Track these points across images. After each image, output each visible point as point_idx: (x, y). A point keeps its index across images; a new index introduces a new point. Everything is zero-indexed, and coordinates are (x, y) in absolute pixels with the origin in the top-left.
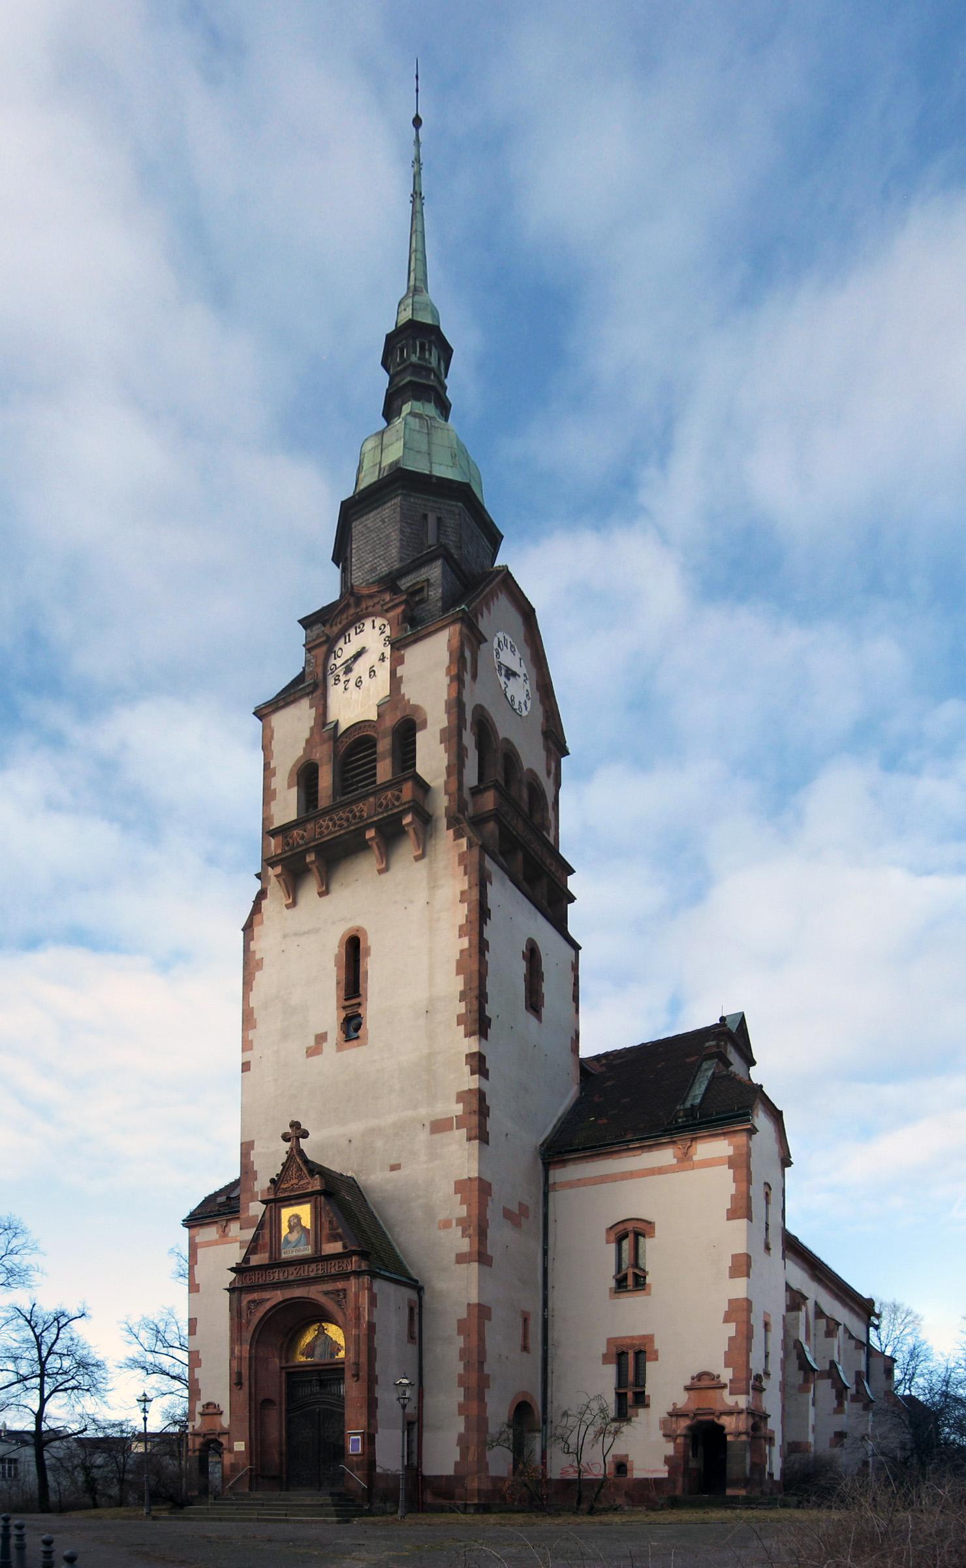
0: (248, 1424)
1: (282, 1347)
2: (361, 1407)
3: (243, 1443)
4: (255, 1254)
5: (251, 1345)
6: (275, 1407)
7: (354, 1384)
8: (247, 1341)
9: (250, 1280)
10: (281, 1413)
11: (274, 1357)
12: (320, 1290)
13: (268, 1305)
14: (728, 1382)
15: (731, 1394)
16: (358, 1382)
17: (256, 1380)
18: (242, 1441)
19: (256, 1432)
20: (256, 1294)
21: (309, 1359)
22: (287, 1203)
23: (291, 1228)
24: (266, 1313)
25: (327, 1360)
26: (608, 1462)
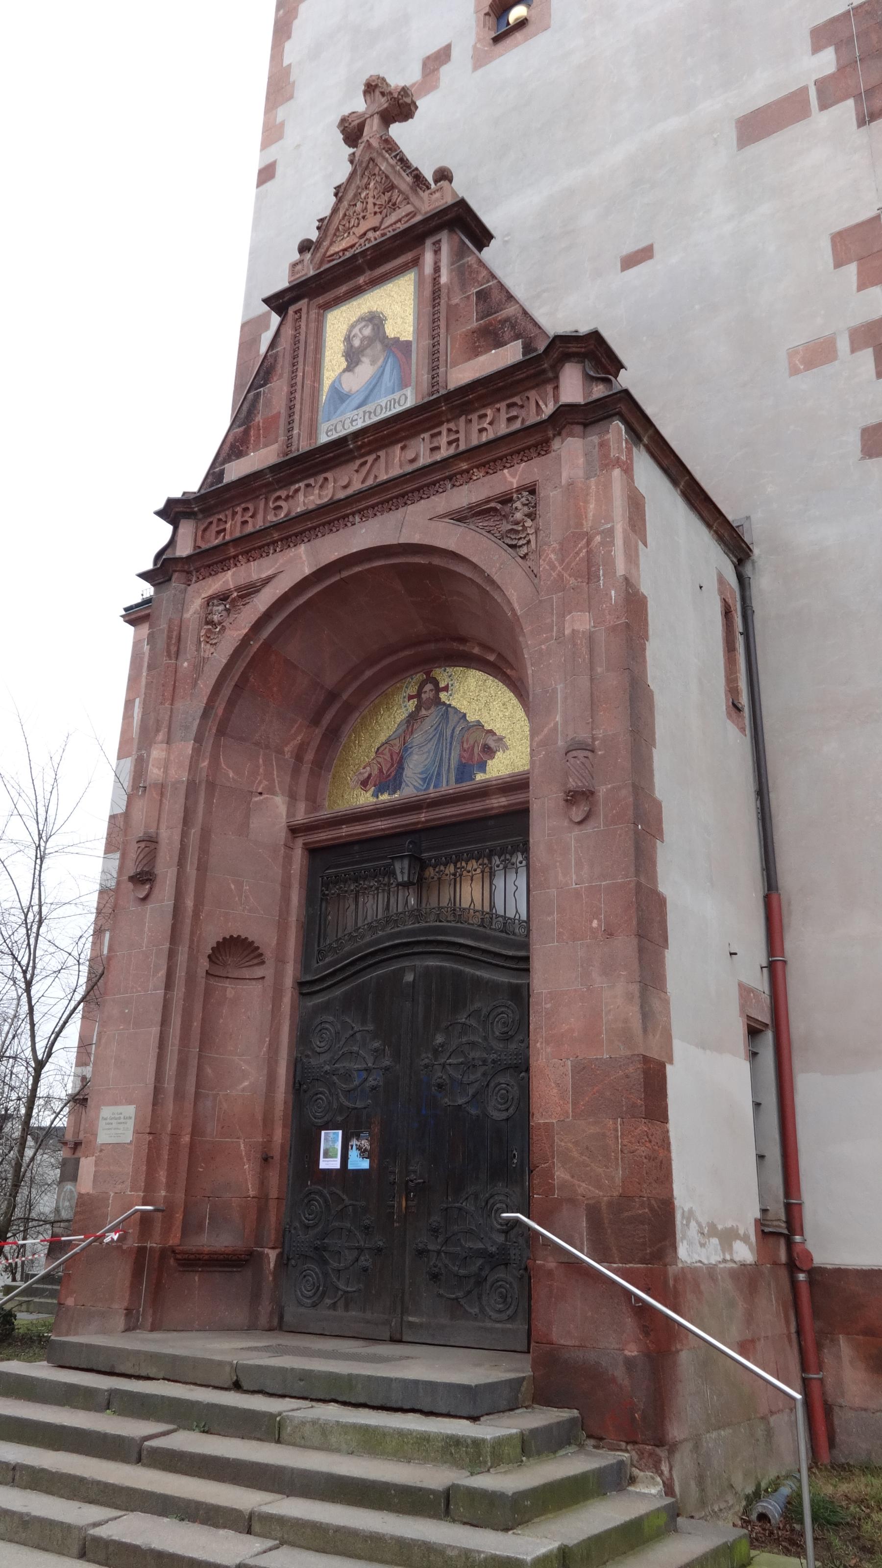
0: (155, 1030)
1: (299, 757)
2: (610, 933)
5: (199, 739)
6: (259, 972)
7: (573, 836)
8: (187, 728)
9: (218, 533)
10: (278, 992)
11: (274, 793)
12: (441, 510)
13: (263, 601)
16: (589, 828)
17: (202, 868)
19: (183, 1064)
20: (230, 573)
21: (385, 797)
24: (258, 626)
25: (448, 786)
26: (336, 1157)
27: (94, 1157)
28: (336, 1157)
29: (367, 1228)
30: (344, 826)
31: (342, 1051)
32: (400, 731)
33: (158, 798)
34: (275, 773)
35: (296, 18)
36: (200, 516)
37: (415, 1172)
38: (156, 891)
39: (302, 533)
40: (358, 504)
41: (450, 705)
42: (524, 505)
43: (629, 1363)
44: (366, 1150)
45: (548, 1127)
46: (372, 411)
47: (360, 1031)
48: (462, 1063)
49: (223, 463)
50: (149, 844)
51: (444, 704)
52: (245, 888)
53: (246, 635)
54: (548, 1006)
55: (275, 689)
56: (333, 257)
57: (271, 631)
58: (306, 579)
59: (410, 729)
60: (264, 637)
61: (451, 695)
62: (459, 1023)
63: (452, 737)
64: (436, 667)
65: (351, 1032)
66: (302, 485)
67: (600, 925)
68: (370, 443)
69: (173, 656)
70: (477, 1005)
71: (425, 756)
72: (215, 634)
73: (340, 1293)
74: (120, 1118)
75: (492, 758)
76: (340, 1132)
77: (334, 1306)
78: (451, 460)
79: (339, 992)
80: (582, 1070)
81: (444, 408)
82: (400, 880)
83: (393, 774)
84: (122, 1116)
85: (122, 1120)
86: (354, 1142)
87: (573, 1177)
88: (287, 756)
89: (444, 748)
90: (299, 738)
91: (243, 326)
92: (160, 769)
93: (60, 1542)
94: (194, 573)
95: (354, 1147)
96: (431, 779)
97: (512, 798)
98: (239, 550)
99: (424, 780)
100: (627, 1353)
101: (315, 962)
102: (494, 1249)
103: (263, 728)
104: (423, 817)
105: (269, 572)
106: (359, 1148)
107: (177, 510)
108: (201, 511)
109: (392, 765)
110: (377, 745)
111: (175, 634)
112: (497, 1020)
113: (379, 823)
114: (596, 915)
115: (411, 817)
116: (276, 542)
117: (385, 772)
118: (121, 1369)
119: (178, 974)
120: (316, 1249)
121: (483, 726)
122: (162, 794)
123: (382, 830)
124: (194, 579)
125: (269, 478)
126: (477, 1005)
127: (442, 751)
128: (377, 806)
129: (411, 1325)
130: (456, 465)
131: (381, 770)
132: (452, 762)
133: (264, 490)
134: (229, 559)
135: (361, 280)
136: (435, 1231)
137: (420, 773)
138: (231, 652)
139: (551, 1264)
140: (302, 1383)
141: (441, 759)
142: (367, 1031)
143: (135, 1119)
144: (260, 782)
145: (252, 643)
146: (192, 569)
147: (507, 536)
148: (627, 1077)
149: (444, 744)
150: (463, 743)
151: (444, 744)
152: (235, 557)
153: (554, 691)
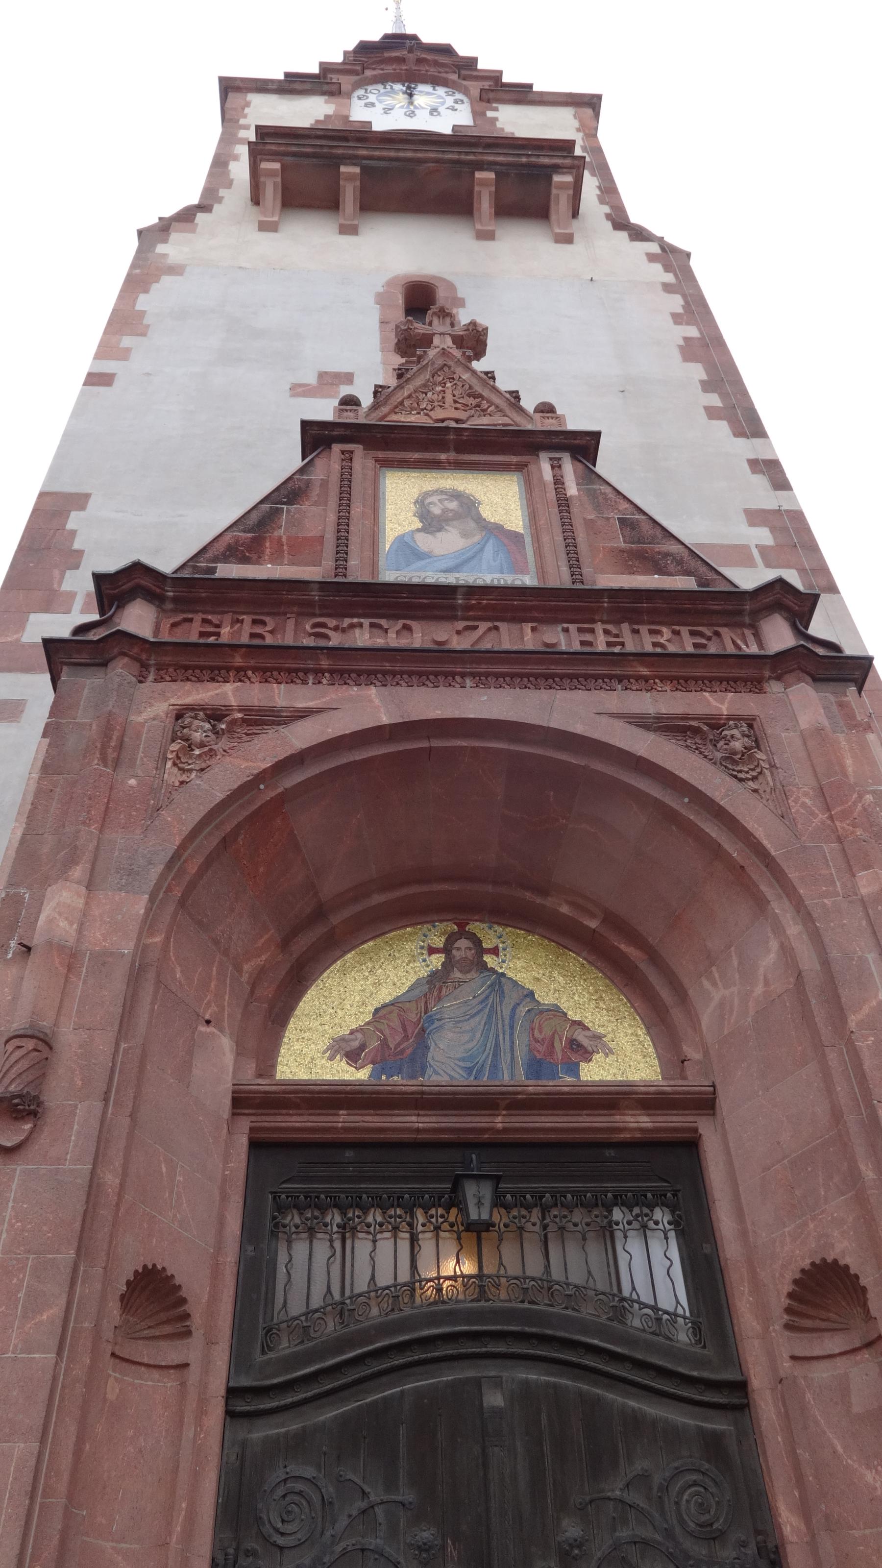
6: (172, 1353)
30: (341, 1112)
31: (343, 1545)
32: (417, 992)
33: (63, 971)
34: (227, 998)
35: (157, 281)
36: (169, 606)
38: (44, 1139)
39: (375, 673)
40: (474, 666)
41: (503, 975)
42: (744, 735)
47: (382, 1503)
49: (216, 559)
50: (41, 1045)
52: (178, 1178)
53: (265, 771)
55: (261, 870)
57: (299, 780)
58: (380, 729)
59: (435, 994)
61: (504, 962)
62: (609, 1499)
63: (512, 1017)
64: (477, 921)
65: (363, 1505)
66: (366, 622)
68: (486, 608)
69: (110, 763)
70: (640, 1465)
71: (467, 1037)
72: (191, 758)
78: (631, 658)
79: (328, 1414)
81: (606, 605)
82: (474, 1216)
83: (409, 1051)
88: (245, 978)
89: (500, 1031)
90: (264, 958)
91: (42, 495)
92: (71, 924)
94: (152, 670)
97: (660, 1119)
98: (252, 663)
99: (469, 1070)
101: (258, 1351)
103: (229, 920)
104: (499, 1121)
105: (311, 704)
107: (143, 582)
108: (175, 600)
109: (406, 1038)
110: (377, 1004)
111: (116, 735)
112: (685, 1497)
113: (414, 1119)
115: (477, 1119)
117: (392, 1046)
119: (72, 1325)
121: (565, 1014)
122: (70, 968)
123: (418, 1130)
124: (151, 677)
125: (316, 596)
126: (640, 1465)
127: (498, 1036)
128: (424, 1088)
130: (632, 666)
131: (384, 1043)
132: (518, 1053)
133: (295, 609)
134: (228, 669)
135: (443, 456)
137: (463, 1059)
138: (235, 787)
141: (497, 1045)
144: (208, 1005)
145: (262, 787)
146: (152, 662)
147: (721, 764)
149: (500, 1026)
150: (533, 1029)
151: (500, 1026)
152: (239, 670)
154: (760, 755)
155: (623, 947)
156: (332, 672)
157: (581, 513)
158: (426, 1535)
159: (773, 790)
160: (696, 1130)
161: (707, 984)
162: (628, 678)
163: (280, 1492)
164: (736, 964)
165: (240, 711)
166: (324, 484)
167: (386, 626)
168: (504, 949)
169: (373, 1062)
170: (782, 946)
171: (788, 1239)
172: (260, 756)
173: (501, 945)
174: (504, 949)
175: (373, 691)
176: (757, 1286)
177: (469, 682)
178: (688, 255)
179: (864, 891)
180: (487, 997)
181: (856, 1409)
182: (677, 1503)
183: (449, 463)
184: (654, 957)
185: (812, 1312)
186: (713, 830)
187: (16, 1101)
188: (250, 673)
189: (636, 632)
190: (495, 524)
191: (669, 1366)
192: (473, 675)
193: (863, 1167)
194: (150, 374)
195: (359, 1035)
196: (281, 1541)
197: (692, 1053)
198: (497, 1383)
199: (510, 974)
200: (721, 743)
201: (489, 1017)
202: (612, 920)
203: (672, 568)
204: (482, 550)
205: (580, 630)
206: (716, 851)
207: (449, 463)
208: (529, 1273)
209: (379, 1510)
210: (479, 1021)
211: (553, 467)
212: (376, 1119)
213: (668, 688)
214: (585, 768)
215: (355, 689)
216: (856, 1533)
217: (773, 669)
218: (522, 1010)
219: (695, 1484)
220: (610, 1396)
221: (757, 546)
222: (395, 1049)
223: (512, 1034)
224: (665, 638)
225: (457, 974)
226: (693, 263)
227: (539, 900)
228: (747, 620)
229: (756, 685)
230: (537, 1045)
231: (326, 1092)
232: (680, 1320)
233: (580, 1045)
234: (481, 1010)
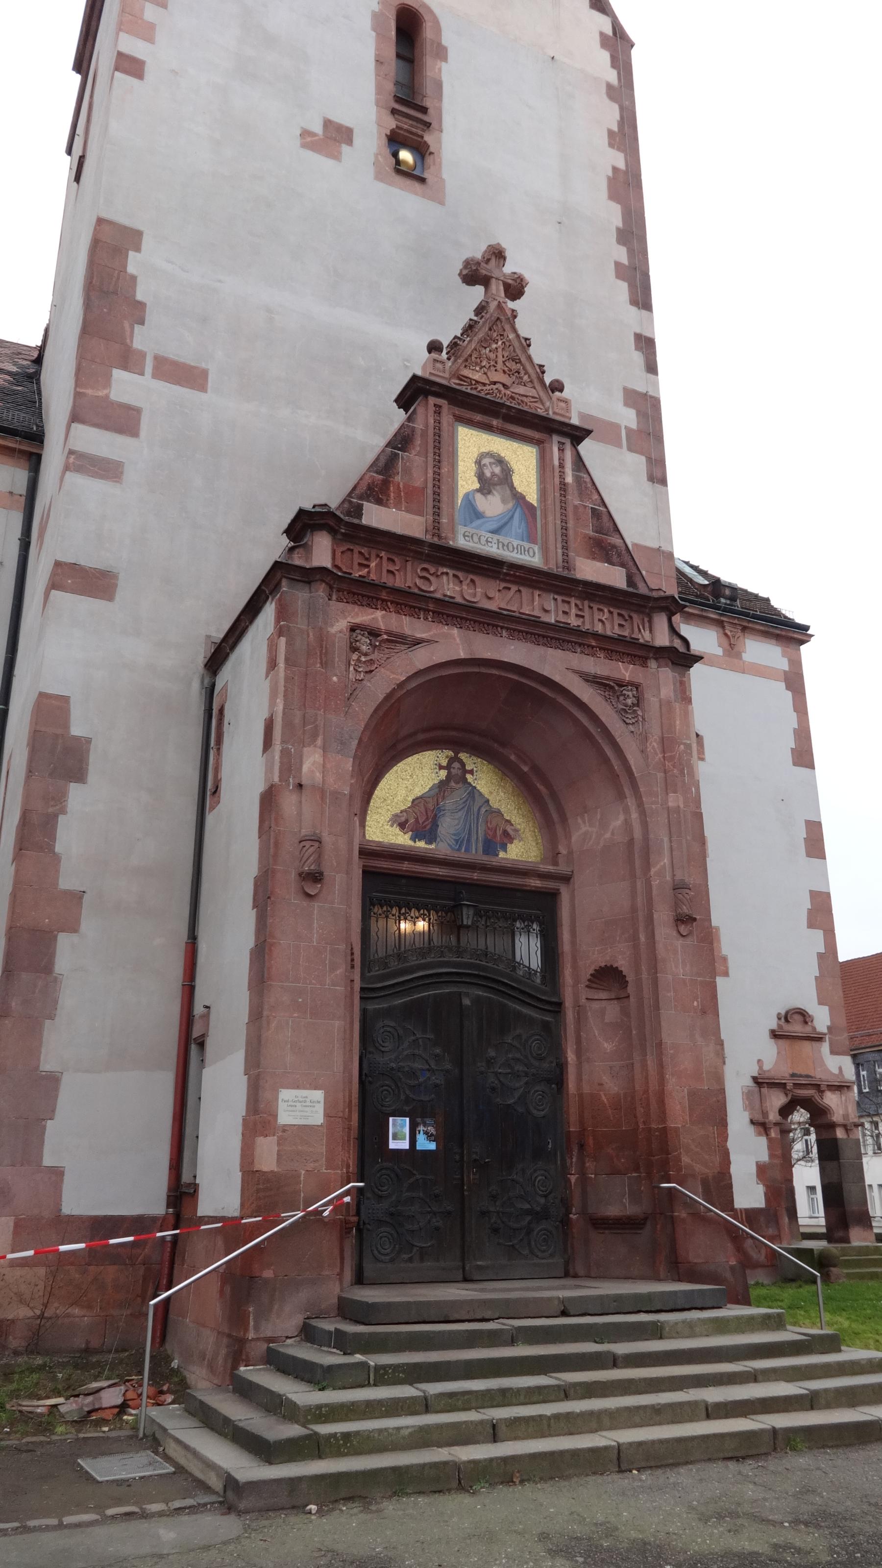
3: (318, 1095)
4: (379, 502)
7: (679, 943)
13: (422, 658)
14: (825, 1031)
15: (833, 1052)
18: (316, 1088)
21: (421, 844)
22: (478, 417)
23: (486, 486)
25: (476, 854)
26: (405, 1139)
27: (275, 1137)
28: (405, 1139)
29: (436, 1196)
32: (432, 793)
36: (339, 537)
37: (476, 1153)
41: (475, 787)
42: (634, 696)
43: (732, 1268)
44: (432, 1135)
45: (676, 1129)
46: (506, 544)
48: (509, 1073)
51: (470, 784)
54: (672, 1052)
56: (466, 380)
59: (442, 794)
60: (409, 688)
61: (476, 779)
65: (413, 1038)
66: (451, 572)
67: (698, 1005)
68: (519, 577)
70: (518, 1032)
73: (415, 1249)
74: (305, 1102)
75: (511, 843)
76: (408, 1119)
77: (410, 1260)
80: (692, 1094)
83: (428, 827)
84: (308, 1100)
85: (308, 1104)
86: (421, 1128)
87: (692, 1161)
93: (690, 1414)
95: (422, 1132)
96: (462, 842)
97: (546, 883)
99: (457, 841)
100: (730, 1263)
102: (538, 1209)
105: (424, 636)
106: (426, 1133)
109: (427, 819)
113: (438, 870)
114: (696, 998)
116: (429, 611)
117: (421, 822)
118: (457, 1316)
120: (392, 1214)
121: (503, 815)
123: (439, 875)
126: (518, 1032)
129: (479, 1268)
131: (417, 820)
133: (411, 554)
134: (378, 599)
135: (495, 422)
136: (494, 1198)
137: (454, 835)
139: (684, 1215)
140: (615, 1304)
142: (429, 1039)
143: (325, 1103)
146: (335, 586)
148: (718, 1101)
150: (487, 822)
152: (383, 600)
153: (662, 840)
154: (640, 713)
155: (538, 785)
156: (434, 612)
157: (573, 499)
158: (438, 1051)
159: (641, 734)
160: (558, 890)
161: (580, 821)
162: (584, 645)
163: (382, 1030)
164: (599, 818)
165: (386, 633)
166: (424, 433)
167: (462, 579)
168: (476, 772)
169: (411, 831)
170: (626, 820)
171: (596, 953)
172: (399, 671)
173: (475, 769)
174: (476, 772)
175: (455, 631)
176: (575, 966)
177: (504, 633)
178: (632, 46)
179: (670, 804)
180: (467, 800)
181: (606, 1021)
182: (531, 1047)
183: (497, 429)
184: (553, 795)
185: (598, 982)
186: (609, 752)
187: (317, 875)
188: (389, 603)
189: (591, 608)
190: (521, 494)
191: (534, 993)
192: (507, 629)
193: (641, 936)
194: (177, 73)
195: (405, 814)
196: (383, 1049)
197: (563, 850)
198: (467, 994)
199: (478, 788)
200: (622, 698)
201: (467, 813)
202: (535, 768)
203: (615, 559)
204: (512, 517)
205: (563, 601)
206: (606, 761)
207: (497, 429)
208: (479, 947)
209: (420, 1041)
210: (461, 814)
211: (559, 449)
212: (421, 867)
213: (602, 656)
214: (554, 699)
215: (446, 627)
216: (597, 1063)
217: (654, 654)
218: (483, 810)
219: (538, 1040)
220: (510, 1004)
221: (626, 427)
222: (423, 823)
223: (477, 824)
224: (605, 617)
225: (453, 784)
226: (634, 52)
227: (501, 750)
228: (647, 610)
229: (643, 661)
230: (489, 831)
231: (403, 853)
232: (538, 974)
233: (508, 834)
234: (463, 807)
